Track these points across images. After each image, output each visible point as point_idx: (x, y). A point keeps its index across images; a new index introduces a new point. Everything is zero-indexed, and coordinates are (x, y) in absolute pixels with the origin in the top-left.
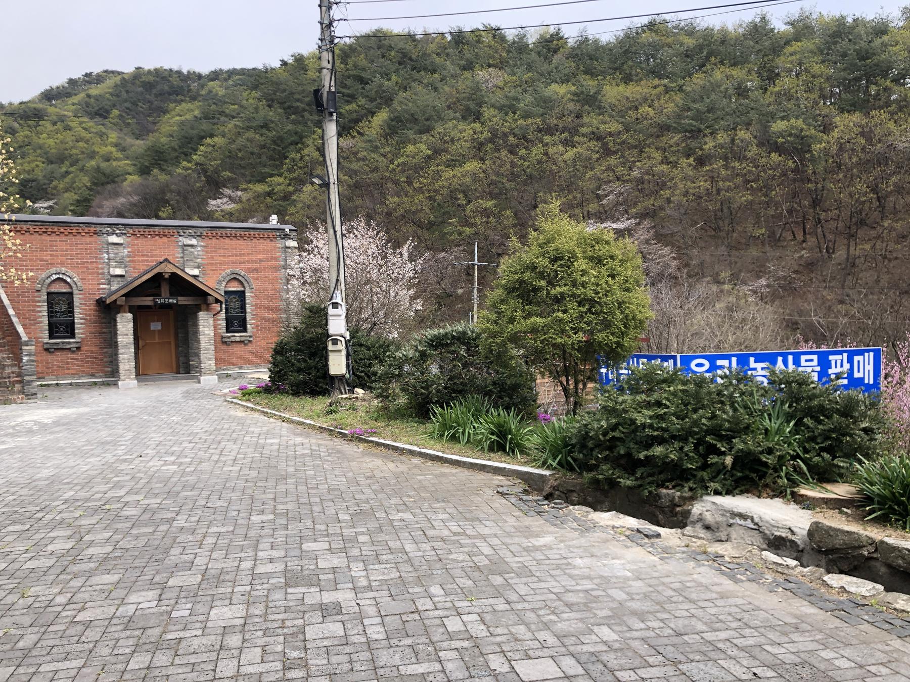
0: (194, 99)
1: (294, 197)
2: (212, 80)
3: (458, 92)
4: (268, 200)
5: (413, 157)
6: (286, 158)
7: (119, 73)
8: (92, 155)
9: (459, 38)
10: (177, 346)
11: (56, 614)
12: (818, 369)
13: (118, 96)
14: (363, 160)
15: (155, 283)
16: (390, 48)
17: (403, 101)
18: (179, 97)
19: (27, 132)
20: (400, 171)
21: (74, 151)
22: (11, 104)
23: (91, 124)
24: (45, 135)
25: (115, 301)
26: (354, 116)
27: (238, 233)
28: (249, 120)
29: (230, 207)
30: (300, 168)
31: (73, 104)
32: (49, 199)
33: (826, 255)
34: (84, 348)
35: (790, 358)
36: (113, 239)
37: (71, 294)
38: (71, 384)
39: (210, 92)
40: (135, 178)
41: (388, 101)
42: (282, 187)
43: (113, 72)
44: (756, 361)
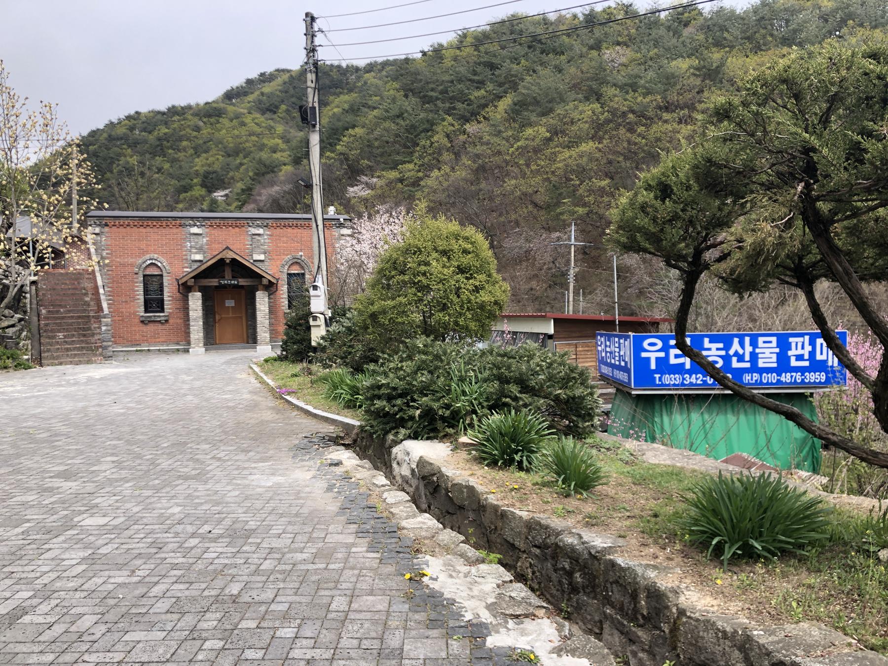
0: (350, 91)
1: (422, 183)
2: (368, 72)
3: (582, 72)
4: (400, 185)
5: (533, 140)
6: (418, 145)
7: (289, 71)
8: (262, 147)
9: (591, 20)
10: (247, 321)
11: (204, 549)
12: (777, 350)
13: (286, 92)
14: (487, 144)
15: (218, 267)
16: (521, 32)
17: (529, 85)
18: (338, 90)
19: (209, 130)
21: (247, 145)
22: (198, 105)
23: (262, 119)
24: (224, 131)
25: (186, 282)
26: (483, 101)
27: (299, 223)
28: (387, 111)
29: (366, 193)
30: (430, 154)
31: (249, 102)
32: (226, 188)
34: (171, 321)
35: (747, 339)
36: (195, 230)
37: (161, 276)
38: (159, 350)
39: (366, 83)
40: (289, 168)
41: (514, 87)
42: (412, 173)
43: (283, 71)
44: (710, 342)
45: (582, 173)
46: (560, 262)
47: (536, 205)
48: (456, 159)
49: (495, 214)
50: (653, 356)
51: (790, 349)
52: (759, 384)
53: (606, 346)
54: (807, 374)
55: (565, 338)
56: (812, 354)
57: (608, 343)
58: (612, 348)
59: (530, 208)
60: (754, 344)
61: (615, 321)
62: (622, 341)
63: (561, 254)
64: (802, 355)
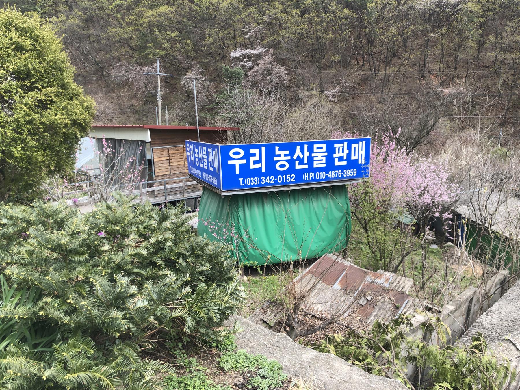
12: (326, 154)
20: (117, 10)
30: (49, 5)
33: (374, 75)
35: (306, 146)
44: (280, 150)
45: (161, 27)
46: (150, 88)
47: (131, 48)
48: (70, 11)
49: (103, 53)
50: (237, 163)
51: (335, 153)
52: (314, 180)
53: (195, 153)
54: (345, 171)
55: (159, 144)
56: (349, 155)
57: (196, 151)
58: (201, 155)
59: (128, 49)
60: (311, 150)
61: (197, 130)
62: (210, 150)
63: (150, 82)
64: (342, 157)
